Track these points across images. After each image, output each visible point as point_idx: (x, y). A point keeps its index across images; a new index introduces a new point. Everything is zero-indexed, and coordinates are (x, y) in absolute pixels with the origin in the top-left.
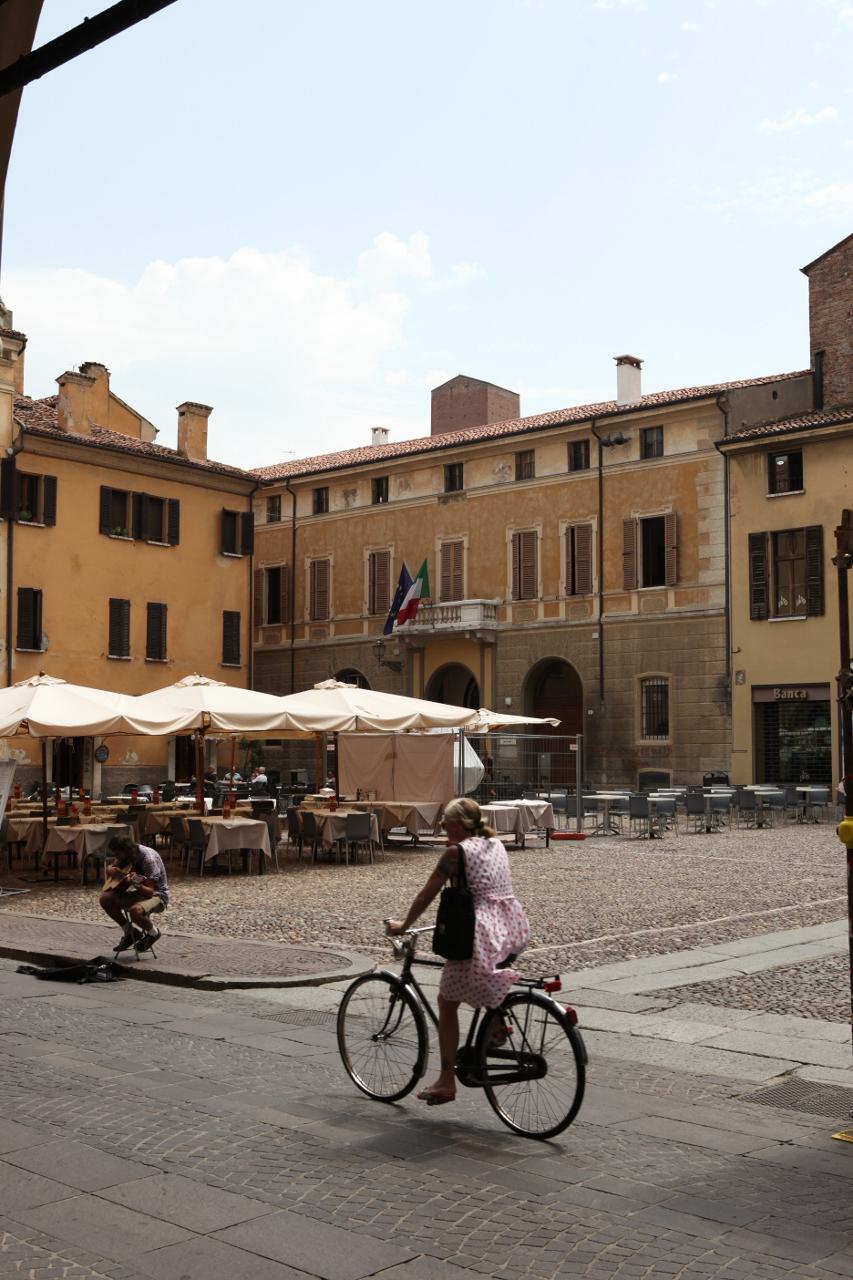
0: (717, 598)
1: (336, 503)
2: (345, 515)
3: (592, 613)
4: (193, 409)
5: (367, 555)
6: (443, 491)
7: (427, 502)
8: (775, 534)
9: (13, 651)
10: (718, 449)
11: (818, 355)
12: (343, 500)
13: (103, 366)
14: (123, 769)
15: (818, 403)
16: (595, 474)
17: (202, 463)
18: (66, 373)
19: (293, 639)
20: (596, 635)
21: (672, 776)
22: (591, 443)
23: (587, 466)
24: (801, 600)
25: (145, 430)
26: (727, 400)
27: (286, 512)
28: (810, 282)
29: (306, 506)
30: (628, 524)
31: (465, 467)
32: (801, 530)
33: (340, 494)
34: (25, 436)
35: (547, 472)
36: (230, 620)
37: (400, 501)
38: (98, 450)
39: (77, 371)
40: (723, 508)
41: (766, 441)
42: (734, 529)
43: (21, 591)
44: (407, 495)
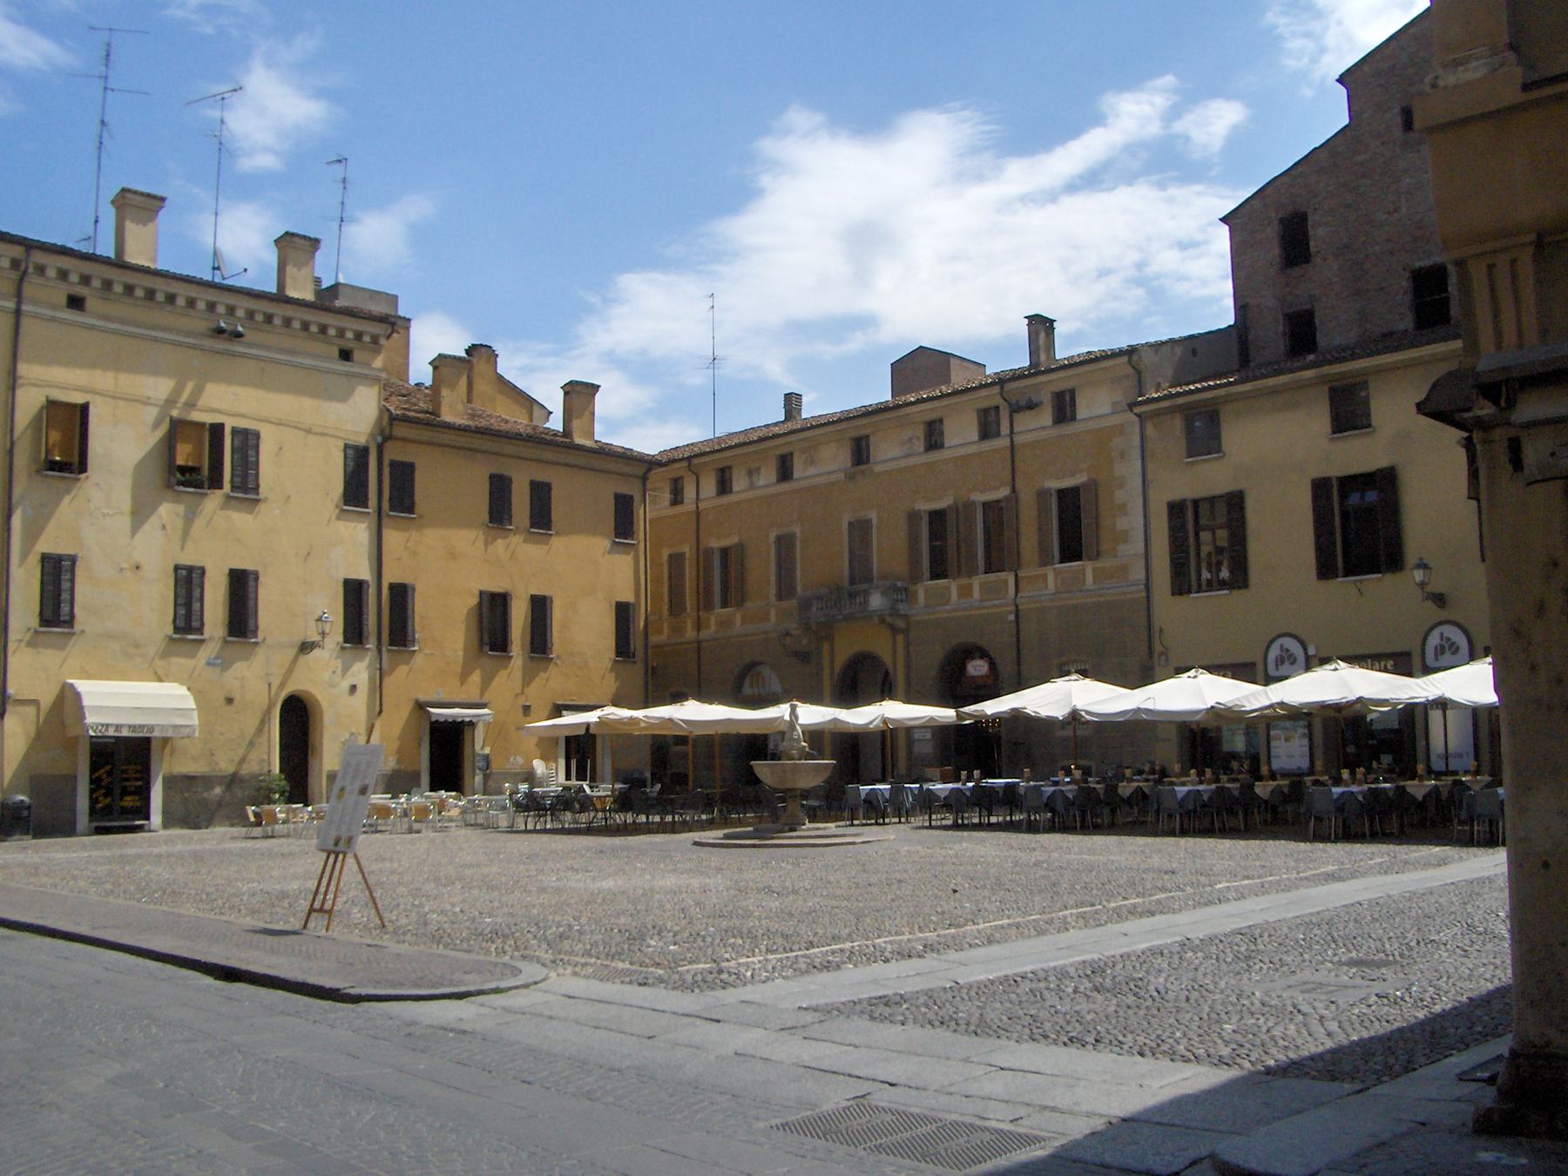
0: (1138, 574)
1: (739, 482)
2: (751, 494)
3: (1007, 593)
4: (578, 388)
5: (773, 536)
6: (850, 465)
7: (833, 478)
8: (1196, 503)
9: (384, 649)
10: (1132, 411)
11: (1241, 307)
12: (747, 478)
13: (490, 347)
14: (507, 773)
15: (1245, 360)
16: (1005, 442)
17: (588, 443)
18: (439, 355)
19: (698, 630)
20: (1012, 617)
21: (1094, 769)
22: (1001, 408)
23: (998, 434)
24: (1225, 574)
25: (536, 411)
26: (1140, 357)
27: (689, 493)
28: (1230, 231)
29: (709, 486)
30: (1042, 494)
31: (872, 439)
32: (1221, 496)
33: (744, 472)
34: (395, 422)
35: (955, 441)
36: (623, 613)
37: (807, 478)
38: (472, 435)
39: (463, 354)
40: (1140, 476)
41: (1181, 400)
42: (1152, 494)
43: (392, 587)
44: (812, 471)
